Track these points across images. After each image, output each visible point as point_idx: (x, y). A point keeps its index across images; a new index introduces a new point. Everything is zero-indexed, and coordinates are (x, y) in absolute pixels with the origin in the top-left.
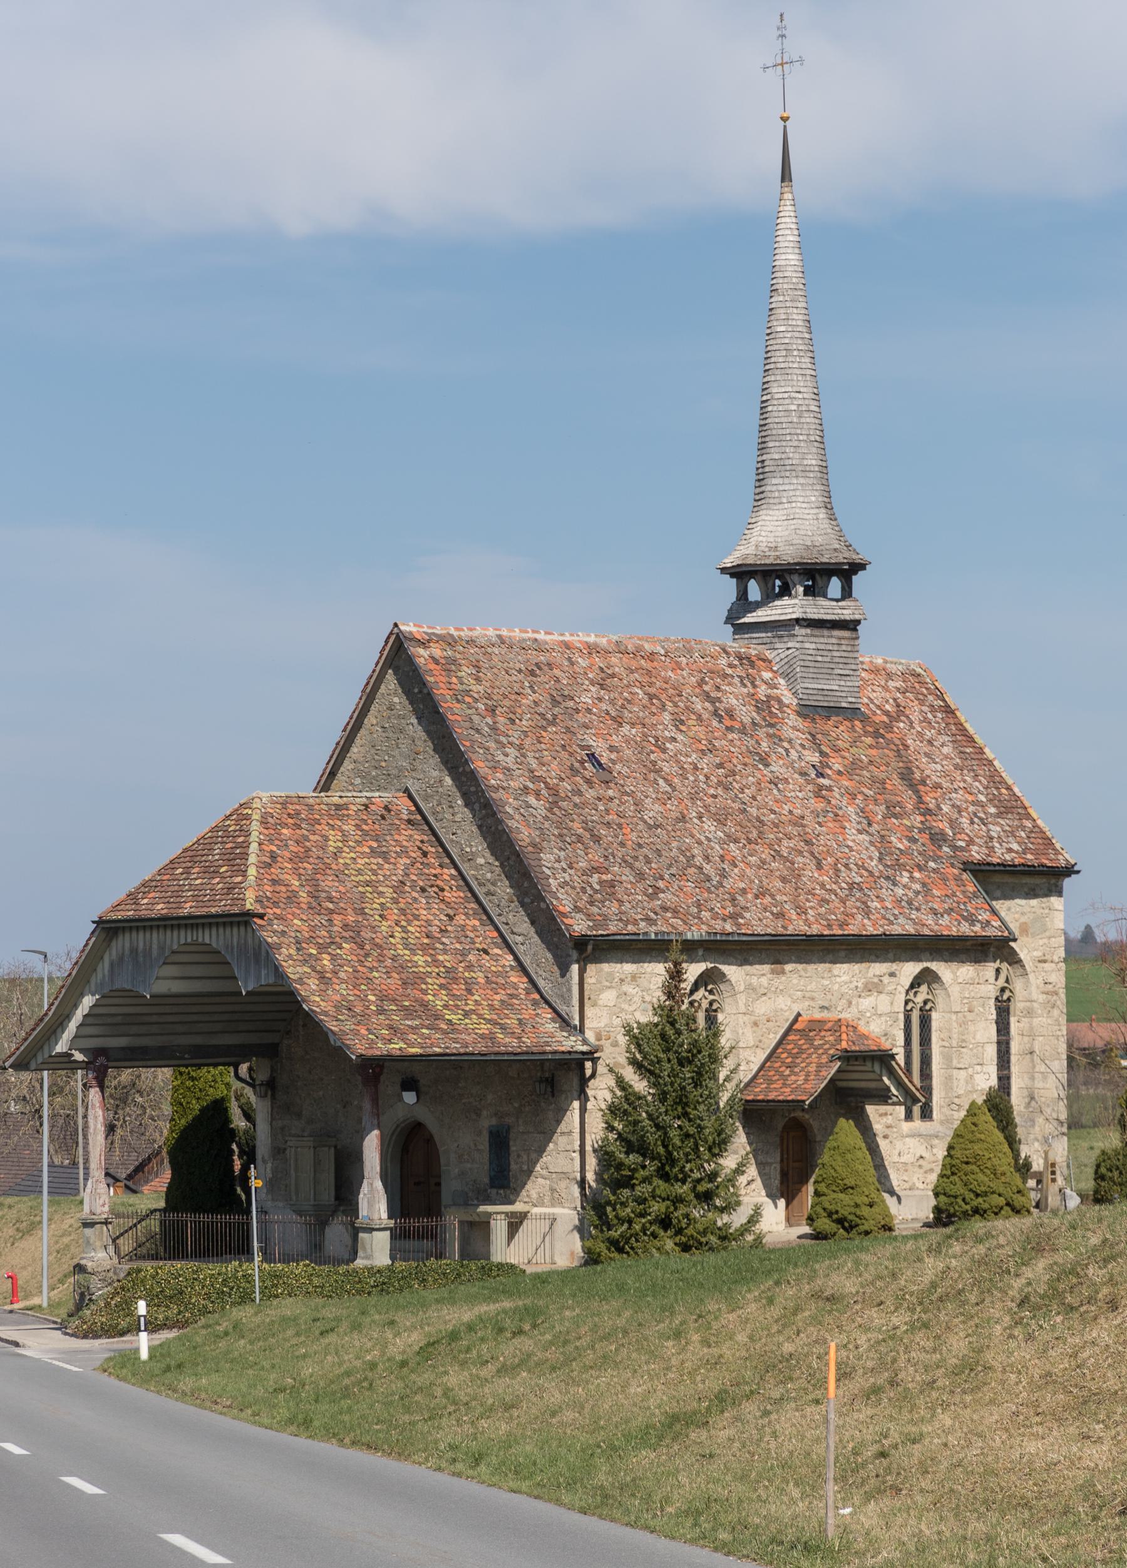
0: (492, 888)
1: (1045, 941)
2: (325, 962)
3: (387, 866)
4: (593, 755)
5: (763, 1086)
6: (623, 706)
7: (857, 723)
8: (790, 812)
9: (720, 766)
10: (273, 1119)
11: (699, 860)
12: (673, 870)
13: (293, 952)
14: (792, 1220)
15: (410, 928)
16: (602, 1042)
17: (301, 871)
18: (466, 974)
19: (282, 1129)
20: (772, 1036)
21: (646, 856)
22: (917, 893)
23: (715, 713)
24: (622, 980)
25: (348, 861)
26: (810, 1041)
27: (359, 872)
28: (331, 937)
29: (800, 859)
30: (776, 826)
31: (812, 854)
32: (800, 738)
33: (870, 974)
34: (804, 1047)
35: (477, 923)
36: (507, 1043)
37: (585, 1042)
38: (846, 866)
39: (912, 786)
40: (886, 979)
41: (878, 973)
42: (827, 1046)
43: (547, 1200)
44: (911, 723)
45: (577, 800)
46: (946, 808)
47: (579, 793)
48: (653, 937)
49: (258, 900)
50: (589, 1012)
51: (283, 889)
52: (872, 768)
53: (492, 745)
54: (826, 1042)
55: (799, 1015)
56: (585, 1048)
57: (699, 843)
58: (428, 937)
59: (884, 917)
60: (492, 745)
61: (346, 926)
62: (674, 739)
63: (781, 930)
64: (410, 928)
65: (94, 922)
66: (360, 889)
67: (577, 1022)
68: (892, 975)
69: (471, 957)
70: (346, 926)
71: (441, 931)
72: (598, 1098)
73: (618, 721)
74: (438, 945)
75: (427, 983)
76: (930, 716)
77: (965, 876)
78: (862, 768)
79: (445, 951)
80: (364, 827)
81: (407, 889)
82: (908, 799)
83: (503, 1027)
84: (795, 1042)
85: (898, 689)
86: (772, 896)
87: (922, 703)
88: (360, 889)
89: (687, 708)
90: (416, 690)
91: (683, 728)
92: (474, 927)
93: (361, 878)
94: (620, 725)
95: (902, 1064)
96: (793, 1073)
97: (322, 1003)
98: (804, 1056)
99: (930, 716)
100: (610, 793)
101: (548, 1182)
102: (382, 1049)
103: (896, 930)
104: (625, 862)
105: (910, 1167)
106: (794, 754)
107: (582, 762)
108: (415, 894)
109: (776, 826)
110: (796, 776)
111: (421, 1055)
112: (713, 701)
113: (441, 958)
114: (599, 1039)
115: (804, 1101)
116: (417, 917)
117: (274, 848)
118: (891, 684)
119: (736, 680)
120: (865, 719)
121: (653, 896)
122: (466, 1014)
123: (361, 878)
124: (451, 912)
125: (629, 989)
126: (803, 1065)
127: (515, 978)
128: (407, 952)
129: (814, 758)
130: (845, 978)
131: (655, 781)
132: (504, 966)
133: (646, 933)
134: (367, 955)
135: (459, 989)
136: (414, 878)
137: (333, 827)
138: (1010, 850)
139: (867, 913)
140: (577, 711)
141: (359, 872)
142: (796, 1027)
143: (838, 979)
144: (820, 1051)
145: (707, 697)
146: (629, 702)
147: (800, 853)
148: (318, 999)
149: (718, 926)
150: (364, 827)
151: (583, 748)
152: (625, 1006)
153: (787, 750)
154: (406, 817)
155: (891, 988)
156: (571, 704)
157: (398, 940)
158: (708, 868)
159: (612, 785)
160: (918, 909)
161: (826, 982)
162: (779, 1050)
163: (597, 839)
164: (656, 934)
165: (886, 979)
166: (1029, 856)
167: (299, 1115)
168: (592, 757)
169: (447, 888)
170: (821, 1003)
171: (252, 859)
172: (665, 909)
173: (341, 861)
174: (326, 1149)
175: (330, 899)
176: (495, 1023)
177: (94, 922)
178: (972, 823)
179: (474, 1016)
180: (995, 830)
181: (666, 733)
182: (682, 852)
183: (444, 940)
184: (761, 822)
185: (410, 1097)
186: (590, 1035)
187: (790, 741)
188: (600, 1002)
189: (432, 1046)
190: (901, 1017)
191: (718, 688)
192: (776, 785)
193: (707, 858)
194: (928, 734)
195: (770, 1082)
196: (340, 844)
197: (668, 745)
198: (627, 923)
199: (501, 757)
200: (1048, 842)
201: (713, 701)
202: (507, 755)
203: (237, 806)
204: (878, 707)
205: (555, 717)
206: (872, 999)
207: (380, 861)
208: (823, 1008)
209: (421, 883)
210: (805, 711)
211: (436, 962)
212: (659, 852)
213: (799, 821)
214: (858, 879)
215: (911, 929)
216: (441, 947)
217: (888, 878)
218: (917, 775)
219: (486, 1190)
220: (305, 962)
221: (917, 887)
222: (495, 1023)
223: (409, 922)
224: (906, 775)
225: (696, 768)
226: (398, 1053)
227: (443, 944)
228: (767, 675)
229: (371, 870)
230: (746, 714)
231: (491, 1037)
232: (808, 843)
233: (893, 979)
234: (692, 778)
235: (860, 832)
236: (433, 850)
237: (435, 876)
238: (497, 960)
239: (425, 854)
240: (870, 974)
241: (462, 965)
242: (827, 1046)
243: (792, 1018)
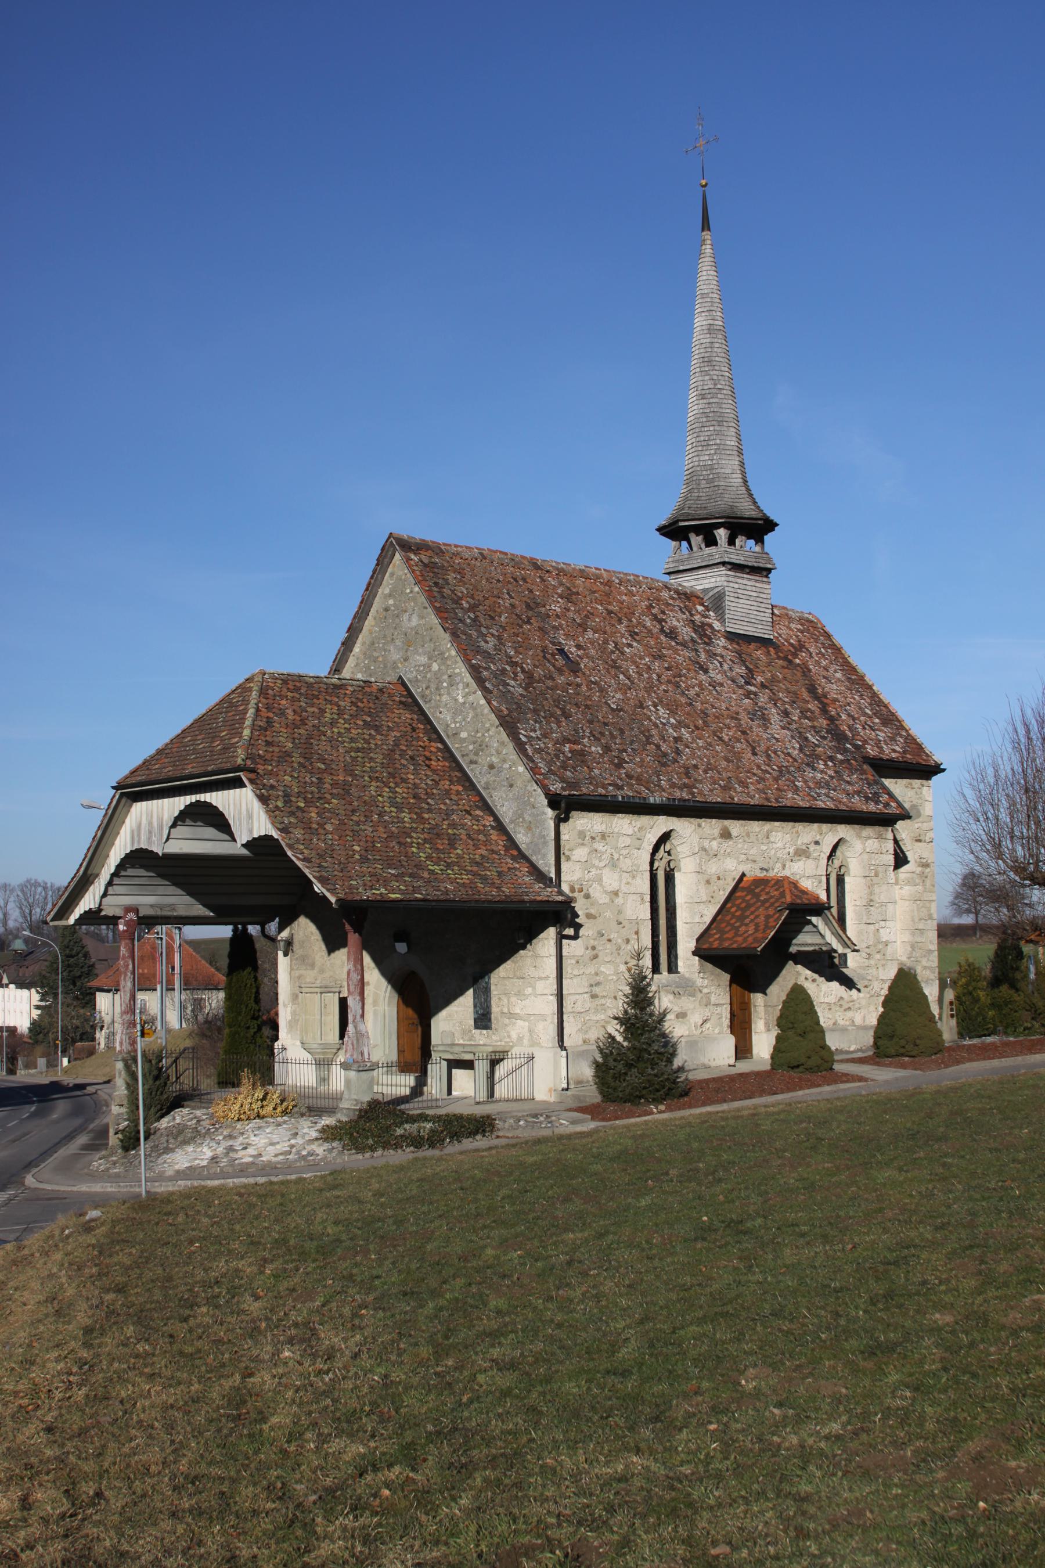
0: (475, 758)
1: (920, 825)
2: (313, 815)
3: (379, 737)
4: (563, 650)
5: (717, 936)
6: (587, 616)
7: (771, 649)
8: (727, 709)
9: (668, 669)
10: (292, 969)
11: (656, 739)
12: (635, 746)
13: (280, 804)
14: (739, 1055)
15: (397, 789)
16: (576, 895)
17: (296, 735)
18: (450, 831)
19: (299, 977)
20: (721, 892)
21: (611, 733)
22: (832, 777)
23: (662, 630)
24: (593, 838)
25: (343, 731)
26: (757, 896)
27: (352, 740)
28: (319, 792)
29: (738, 745)
30: (717, 718)
31: (748, 742)
32: (729, 656)
33: (799, 842)
34: (752, 902)
35: (461, 788)
36: (488, 892)
37: (560, 893)
38: (775, 753)
39: (817, 697)
40: (812, 847)
41: (805, 841)
42: (772, 900)
43: (526, 1042)
44: (811, 654)
45: (550, 683)
46: (844, 717)
47: (552, 678)
48: (620, 799)
49: (249, 757)
50: (565, 866)
51: (277, 749)
52: (785, 682)
53: (474, 634)
54: (772, 897)
55: (743, 875)
56: (560, 898)
57: (656, 726)
58: (414, 798)
59: (809, 795)
60: (474, 634)
61: (335, 784)
62: (630, 646)
63: (728, 800)
64: (397, 789)
65: (113, 788)
66: (353, 754)
67: (553, 875)
68: (817, 843)
69: (454, 817)
70: (335, 784)
71: (427, 794)
72: (746, 582)
73: (583, 627)
74: (423, 805)
75: (411, 837)
76: (823, 650)
77: (865, 767)
78: (779, 682)
79: (430, 811)
80: (359, 704)
81: (397, 756)
82: (813, 706)
83: (484, 879)
84: (743, 898)
85: (798, 630)
86: (719, 773)
87: (816, 641)
88: (353, 754)
89: (639, 623)
90: (408, 591)
91: (637, 638)
92: (458, 793)
93: (353, 745)
94: (585, 630)
95: (836, 915)
96: (742, 924)
97: (305, 851)
98: (752, 909)
99: (823, 650)
100: (578, 680)
101: (527, 1024)
102: (366, 895)
103: (821, 804)
104: (594, 736)
105: (833, 1006)
106: (726, 667)
107: (553, 655)
108: (403, 762)
109: (717, 718)
110: (729, 682)
111: (401, 900)
112: (660, 621)
113: (426, 816)
114: (572, 890)
115: (756, 948)
116: (404, 781)
117: (271, 715)
118: (793, 626)
119: (677, 608)
120: (777, 647)
121: (619, 766)
122: (448, 866)
123: (353, 745)
124: (437, 778)
125: (599, 846)
126: (752, 917)
127: (494, 835)
128: (393, 809)
129: (742, 670)
130: (780, 845)
131: (616, 676)
132: (484, 826)
133: (615, 796)
134: (354, 811)
135: (442, 844)
136: (404, 748)
137: (331, 702)
138: (894, 751)
139: (796, 790)
140: (548, 616)
141: (352, 740)
142: (741, 885)
143: (775, 846)
144: (767, 905)
145: (655, 618)
146: (592, 614)
147: (738, 741)
148: (302, 847)
149: (678, 794)
150: (359, 704)
151: (554, 644)
152: (596, 862)
153: (720, 663)
154: (398, 699)
155: (815, 855)
156: (543, 610)
157: (386, 799)
158: (664, 747)
159: (580, 674)
160: (835, 790)
161: (764, 848)
162: (729, 905)
163: (567, 715)
164: (623, 797)
165: (812, 847)
166: (908, 756)
167: (312, 966)
168: (561, 651)
169: (433, 758)
170: (761, 865)
171: (248, 723)
172: (629, 776)
173: (336, 730)
174: (331, 994)
175: (323, 760)
176: (475, 874)
177: (113, 788)
178: (864, 728)
179: (456, 868)
180: (881, 736)
181: (624, 641)
182: (642, 732)
183: (429, 800)
184: (705, 714)
185: (402, 948)
186: (565, 888)
187: (722, 657)
188: (573, 858)
189: (414, 892)
190: (824, 879)
191: (663, 613)
192: (714, 687)
193: (663, 738)
194: (824, 663)
195: (722, 932)
196: (336, 717)
197: (626, 649)
198: (597, 786)
199: (483, 643)
200: (920, 747)
201: (660, 621)
202: (487, 642)
203: (242, 680)
204: (786, 640)
205: (529, 618)
206: (801, 863)
207: (373, 732)
208: (762, 869)
209: (410, 753)
210: (731, 636)
211: (421, 819)
212: (622, 731)
213: (735, 717)
214: (785, 764)
215: (831, 805)
216: (427, 806)
217: (808, 765)
218: (820, 691)
219: (470, 1031)
220: (292, 814)
221: (831, 772)
222: (475, 874)
223: (397, 785)
224: (812, 689)
225: (649, 668)
226: (379, 898)
227: (428, 804)
228: (700, 608)
229: (364, 739)
230: (686, 632)
231: (472, 885)
232: (744, 733)
233: (818, 847)
234: (646, 676)
235: (783, 728)
236: (422, 727)
237: (423, 748)
238: (478, 820)
239: (414, 730)
240: (799, 842)
241: (446, 822)
242: (772, 900)
243: (737, 877)
